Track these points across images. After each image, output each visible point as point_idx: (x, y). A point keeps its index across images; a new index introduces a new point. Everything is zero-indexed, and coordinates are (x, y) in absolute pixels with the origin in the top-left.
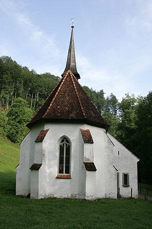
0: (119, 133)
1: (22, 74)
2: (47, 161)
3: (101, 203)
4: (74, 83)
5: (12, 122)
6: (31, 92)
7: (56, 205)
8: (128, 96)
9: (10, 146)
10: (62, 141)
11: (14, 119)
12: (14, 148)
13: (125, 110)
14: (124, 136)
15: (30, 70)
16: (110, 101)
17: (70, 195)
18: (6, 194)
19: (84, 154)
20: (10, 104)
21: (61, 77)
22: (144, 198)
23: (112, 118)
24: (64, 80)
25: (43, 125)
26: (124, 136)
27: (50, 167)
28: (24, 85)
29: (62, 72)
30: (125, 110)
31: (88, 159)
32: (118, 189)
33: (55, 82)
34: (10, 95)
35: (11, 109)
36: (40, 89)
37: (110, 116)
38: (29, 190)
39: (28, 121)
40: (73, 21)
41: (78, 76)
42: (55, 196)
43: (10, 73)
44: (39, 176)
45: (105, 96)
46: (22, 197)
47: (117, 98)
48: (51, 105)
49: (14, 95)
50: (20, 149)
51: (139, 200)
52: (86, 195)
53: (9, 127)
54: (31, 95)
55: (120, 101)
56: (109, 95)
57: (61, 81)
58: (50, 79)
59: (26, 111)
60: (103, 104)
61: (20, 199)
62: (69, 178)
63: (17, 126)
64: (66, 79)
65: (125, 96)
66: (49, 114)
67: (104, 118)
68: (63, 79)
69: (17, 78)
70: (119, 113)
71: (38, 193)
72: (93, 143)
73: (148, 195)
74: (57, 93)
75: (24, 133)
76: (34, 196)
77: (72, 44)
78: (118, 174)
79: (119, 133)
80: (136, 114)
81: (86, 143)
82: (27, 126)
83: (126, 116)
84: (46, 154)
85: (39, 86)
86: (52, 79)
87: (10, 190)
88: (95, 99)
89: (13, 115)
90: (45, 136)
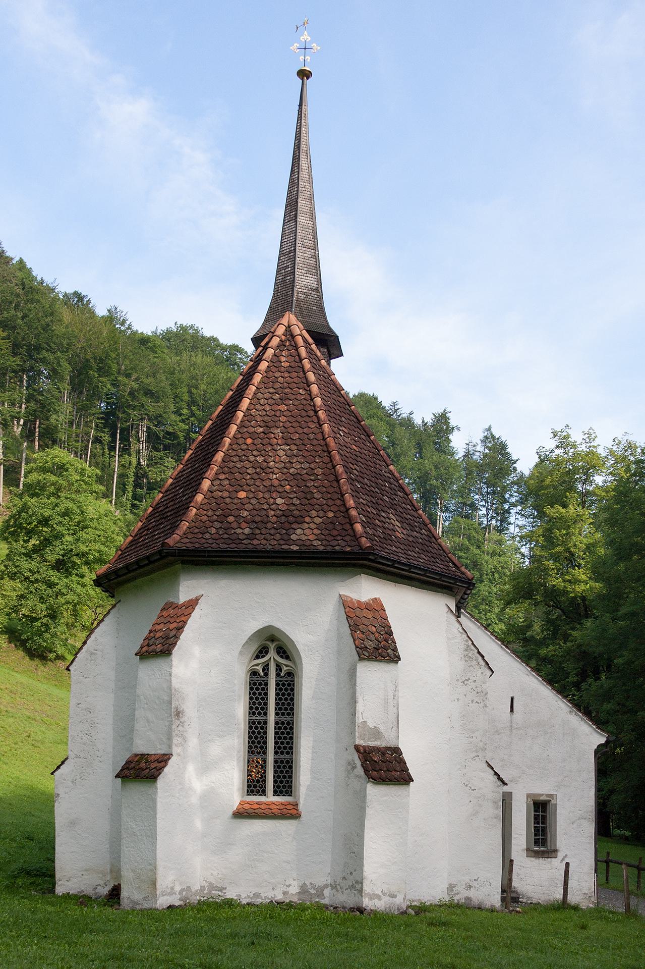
0: (518, 614)
1: (58, 329)
2: (193, 742)
3: (431, 924)
4: (311, 377)
5: (26, 565)
6: (109, 421)
7: (234, 935)
8: (564, 442)
10: (262, 652)
11: (36, 550)
12: (42, 687)
13: (548, 510)
14: (537, 627)
15: (101, 311)
16: (481, 468)
17: (294, 890)
18: (12, 889)
19: (360, 707)
21: (250, 348)
22: (622, 910)
23: (488, 546)
24: (263, 366)
25: (174, 580)
26: (537, 627)
27: (205, 768)
28: (77, 386)
29: (255, 325)
30: (548, 510)
31: (376, 733)
32: (508, 865)
33: (223, 374)
36: (152, 407)
38: (116, 871)
39: (100, 561)
42: (231, 894)
45: (458, 443)
46: (83, 900)
47: (513, 451)
49: (28, 435)
51: (598, 912)
52: (367, 888)
54: (113, 436)
57: (253, 370)
58: (199, 359)
59: (91, 511)
60: (446, 481)
61: (75, 911)
62: (291, 813)
63: (51, 585)
64: (275, 362)
66: (199, 528)
67: (447, 543)
68: (258, 360)
69: (38, 348)
71: (154, 883)
72: (395, 658)
73: (637, 896)
74: (233, 428)
75: (87, 615)
76: (137, 896)
77: (304, 175)
78: (507, 801)
79: (518, 614)
80: (597, 526)
81: (370, 658)
82: (98, 582)
83: (548, 630)
84: (190, 709)
85: (148, 393)
86: (209, 360)
87: (28, 873)
88: (410, 459)
89: (30, 533)
90: (180, 629)
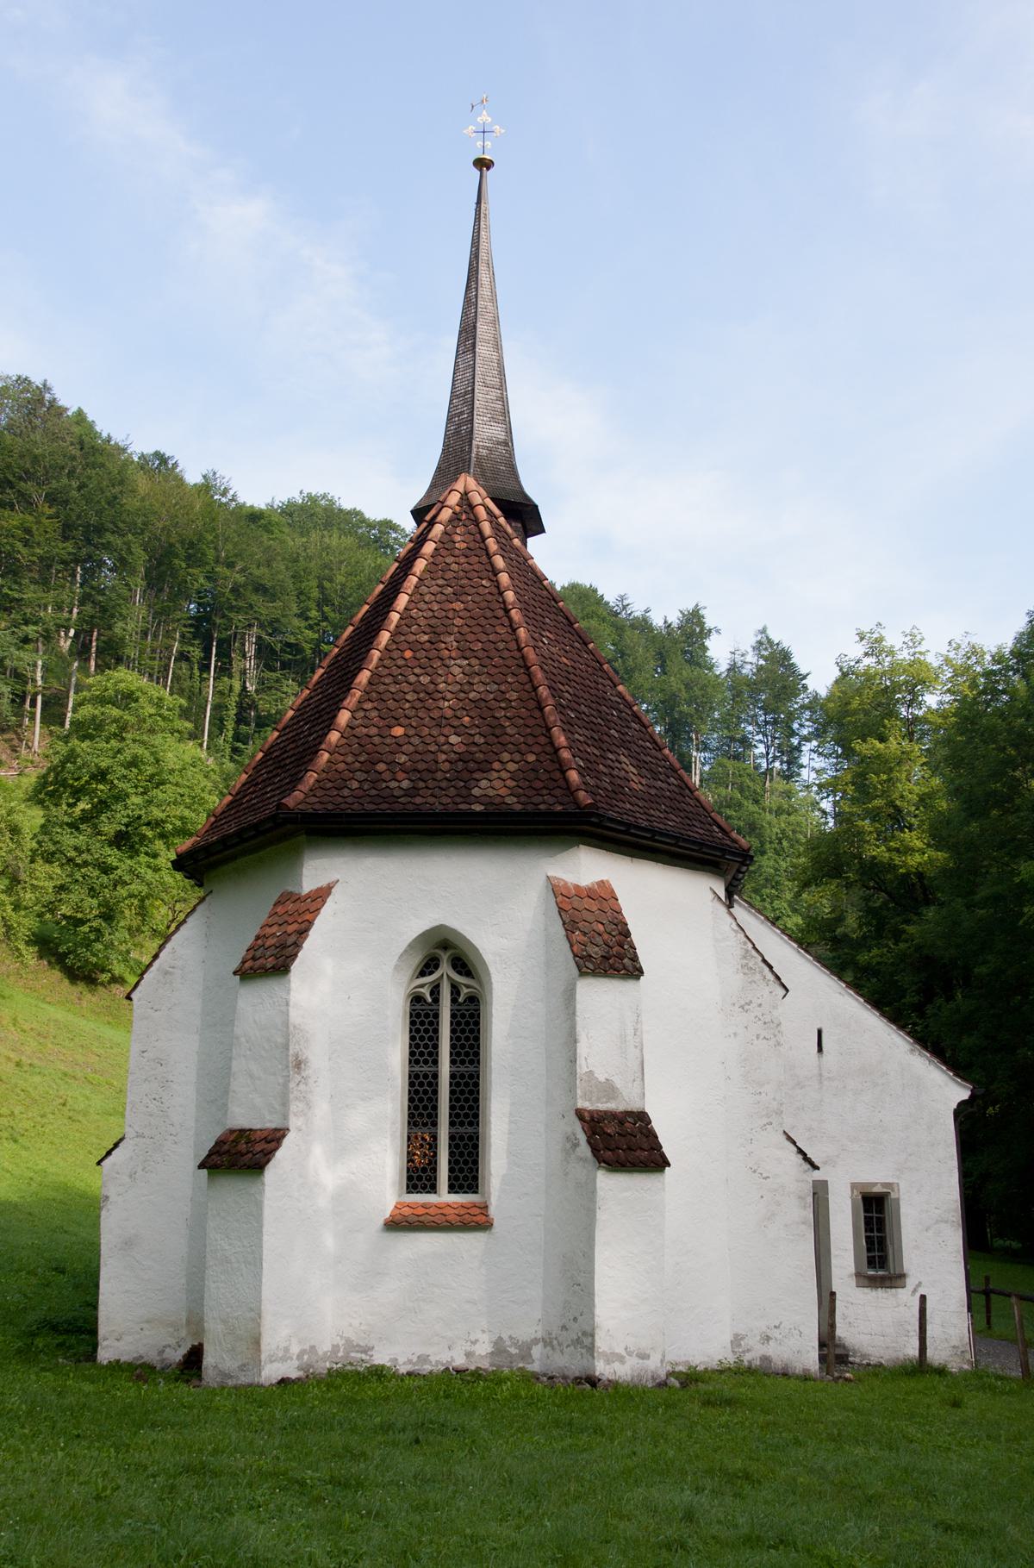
0: (822, 900)
1: (130, 503)
2: (322, 1109)
3: (707, 1403)
4: (499, 562)
5: (69, 840)
6: (201, 629)
7: (386, 1428)
8: (876, 647)
9: (58, 1014)
10: (429, 966)
11: (86, 817)
12: (87, 1025)
13: (858, 745)
15: (193, 477)
16: (754, 686)
17: (483, 1348)
18: (26, 1355)
19: (582, 1049)
20: (54, 711)
21: (409, 525)
22: (1017, 1373)
23: (770, 801)
24: (429, 548)
25: (293, 858)
26: (851, 921)
29: (417, 492)
30: (858, 745)
31: (610, 1090)
32: (827, 1301)
33: (370, 560)
34: (52, 650)
35: (62, 749)
36: (265, 609)
37: (751, 786)
39: (183, 832)
40: (484, 118)
41: (525, 516)
42: (381, 1358)
43: (51, 499)
44: (267, 1212)
45: (719, 652)
46: (140, 1371)
48: (344, 717)
50: (128, 1025)
51: (978, 1378)
52: (602, 1343)
53: (47, 876)
54: (207, 651)
55: (820, 679)
56: (747, 642)
57: (414, 554)
58: (334, 540)
59: (171, 759)
60: (703, 705)
61: (128, 1391)
62: (476, 1221)
63: (106, 869)
64: (446, 542)
65: (856, 650)
66: (334, 780)
67: (709, 797)
68: (420, 540)
70: (814, 764)
71: (257, 1342)
74: (385, 637)
75: (161, 914)
76: (230, 1364)
77: (484, 291)
78: (820, 1195)
79: (822, 900)
82: (178, 865)
84: (317, 1057)
85: (260, 589)
86: (349, 541)
88: (648, 675)
89: (78, 793)
